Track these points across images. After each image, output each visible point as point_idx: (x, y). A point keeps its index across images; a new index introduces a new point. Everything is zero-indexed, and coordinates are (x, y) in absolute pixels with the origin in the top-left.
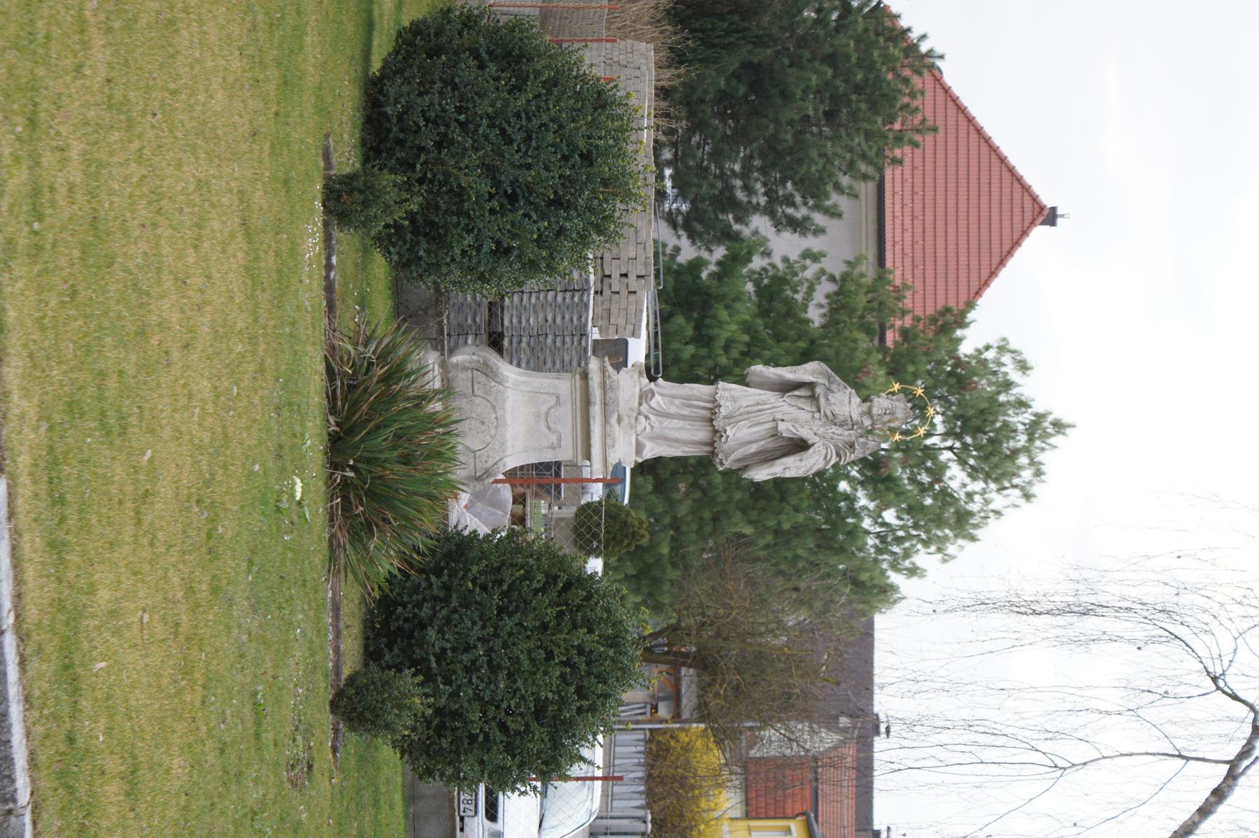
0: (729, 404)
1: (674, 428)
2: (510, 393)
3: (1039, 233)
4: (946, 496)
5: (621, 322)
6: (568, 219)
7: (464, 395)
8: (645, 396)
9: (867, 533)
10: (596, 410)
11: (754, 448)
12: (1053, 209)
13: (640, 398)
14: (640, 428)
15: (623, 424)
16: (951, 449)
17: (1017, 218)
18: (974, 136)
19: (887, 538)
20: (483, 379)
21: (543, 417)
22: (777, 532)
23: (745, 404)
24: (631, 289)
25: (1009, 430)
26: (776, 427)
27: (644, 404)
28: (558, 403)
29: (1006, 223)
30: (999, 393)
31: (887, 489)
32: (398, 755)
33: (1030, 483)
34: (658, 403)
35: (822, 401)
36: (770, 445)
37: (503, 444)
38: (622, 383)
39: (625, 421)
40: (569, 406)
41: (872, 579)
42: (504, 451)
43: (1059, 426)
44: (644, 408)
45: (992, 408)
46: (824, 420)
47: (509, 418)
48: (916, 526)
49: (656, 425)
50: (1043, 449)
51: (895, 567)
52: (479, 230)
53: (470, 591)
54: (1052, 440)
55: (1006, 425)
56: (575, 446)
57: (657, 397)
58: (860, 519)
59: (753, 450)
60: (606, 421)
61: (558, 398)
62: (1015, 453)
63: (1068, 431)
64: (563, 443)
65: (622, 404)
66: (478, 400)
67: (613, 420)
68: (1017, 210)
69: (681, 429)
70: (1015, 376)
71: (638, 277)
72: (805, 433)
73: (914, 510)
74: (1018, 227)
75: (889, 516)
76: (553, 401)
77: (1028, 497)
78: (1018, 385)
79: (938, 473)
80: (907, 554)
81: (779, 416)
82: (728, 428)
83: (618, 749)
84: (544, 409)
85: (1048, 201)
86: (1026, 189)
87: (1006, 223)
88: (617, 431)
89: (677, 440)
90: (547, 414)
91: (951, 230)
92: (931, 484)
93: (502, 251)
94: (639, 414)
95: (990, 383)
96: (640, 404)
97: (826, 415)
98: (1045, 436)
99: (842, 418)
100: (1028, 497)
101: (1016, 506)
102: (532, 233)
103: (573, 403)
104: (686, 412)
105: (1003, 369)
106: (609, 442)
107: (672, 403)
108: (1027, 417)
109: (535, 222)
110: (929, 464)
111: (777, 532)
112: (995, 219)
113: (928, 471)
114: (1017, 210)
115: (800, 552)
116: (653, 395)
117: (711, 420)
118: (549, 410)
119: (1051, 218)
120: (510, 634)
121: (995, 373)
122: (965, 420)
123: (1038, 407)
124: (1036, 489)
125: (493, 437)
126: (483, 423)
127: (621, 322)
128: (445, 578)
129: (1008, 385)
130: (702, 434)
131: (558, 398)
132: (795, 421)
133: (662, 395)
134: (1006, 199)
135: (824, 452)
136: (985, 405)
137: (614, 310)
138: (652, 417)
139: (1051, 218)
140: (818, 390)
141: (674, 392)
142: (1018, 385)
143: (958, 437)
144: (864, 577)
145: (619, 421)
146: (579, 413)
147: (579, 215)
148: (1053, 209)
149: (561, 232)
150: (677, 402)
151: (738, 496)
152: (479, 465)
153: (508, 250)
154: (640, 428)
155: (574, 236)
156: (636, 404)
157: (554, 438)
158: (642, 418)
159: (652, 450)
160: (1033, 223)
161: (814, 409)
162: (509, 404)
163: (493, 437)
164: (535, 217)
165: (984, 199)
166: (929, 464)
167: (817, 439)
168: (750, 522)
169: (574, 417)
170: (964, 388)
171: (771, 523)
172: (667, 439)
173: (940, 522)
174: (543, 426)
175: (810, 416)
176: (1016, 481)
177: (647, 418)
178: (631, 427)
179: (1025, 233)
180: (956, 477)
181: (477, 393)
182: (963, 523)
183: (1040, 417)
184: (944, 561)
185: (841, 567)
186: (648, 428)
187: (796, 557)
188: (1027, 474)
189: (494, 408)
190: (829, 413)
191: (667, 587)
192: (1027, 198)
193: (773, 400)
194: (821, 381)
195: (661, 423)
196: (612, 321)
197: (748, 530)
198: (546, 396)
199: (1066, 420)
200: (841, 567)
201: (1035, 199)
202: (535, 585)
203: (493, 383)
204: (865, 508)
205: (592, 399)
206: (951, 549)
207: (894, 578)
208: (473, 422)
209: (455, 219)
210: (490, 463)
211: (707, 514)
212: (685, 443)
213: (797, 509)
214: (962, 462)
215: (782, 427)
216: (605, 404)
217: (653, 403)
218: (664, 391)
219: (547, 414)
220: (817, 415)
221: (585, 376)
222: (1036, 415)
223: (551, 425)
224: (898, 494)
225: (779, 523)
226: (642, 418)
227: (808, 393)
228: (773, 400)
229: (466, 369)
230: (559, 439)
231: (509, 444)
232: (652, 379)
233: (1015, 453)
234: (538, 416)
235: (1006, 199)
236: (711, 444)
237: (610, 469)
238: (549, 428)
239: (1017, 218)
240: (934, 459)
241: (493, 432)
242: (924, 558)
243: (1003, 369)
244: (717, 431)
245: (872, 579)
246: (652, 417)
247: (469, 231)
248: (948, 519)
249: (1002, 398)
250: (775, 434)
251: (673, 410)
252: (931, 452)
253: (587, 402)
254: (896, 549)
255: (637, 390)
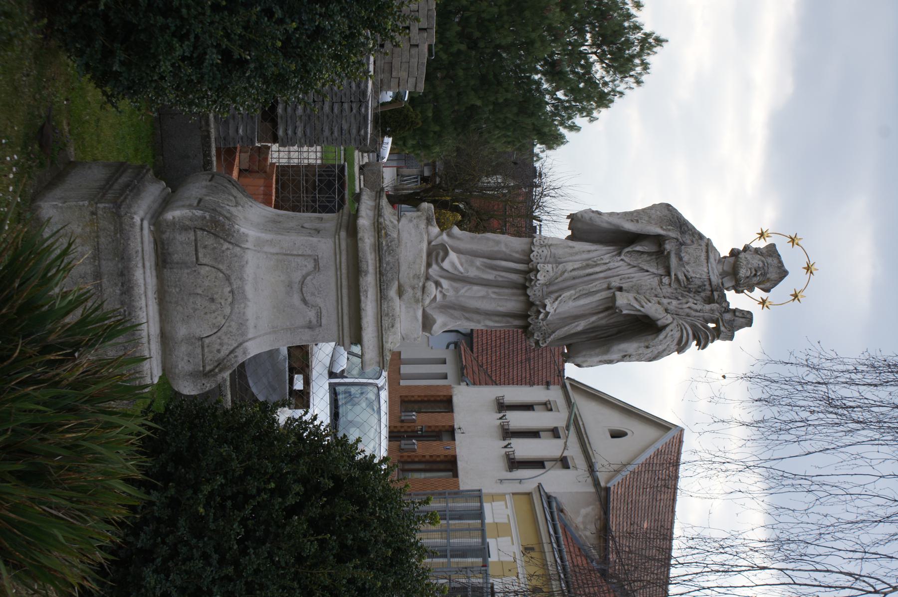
0: (549, 267)
1: (474, 296)
2: (250, 256)
4: (591, 82)
5: (403, 75)
6: (328, 16)
7: (183, 264)
8: (436, 253)
9: (548, 103)
10: (369, 281)
11: (581, 325)
13: (429, 255)
15: (405, 297)
16: (595, 53)
19: (559, 105)
20: (210, 241)
21: (296, 287)
22: (495, 104)
23: (570, 266)
24: (413, 42)
25: (629, 44)
26: (613, 298)
27: (434, 266)
28: (317, 267)
30: (625, 21)
31: (560, 79)
33: (640, 74)
35: (674, 261)
36: (603, 322)
37: (242, 325)
38: (405, 236)
39: (409, 293)
40: (331, 273)
41: (550, 131)
42: (243, 334)
43: (659, 41)
44: (434, 270)
45: (620, 31)
46: (674, 285)
47: (249, 289)
48: (575, 101)
49: (450, 294)
50: (649, 54)
51: (562, 124)
52: (197, 37)
53: (202, 518)
54: (655, 49)
55: (627, 40)
57: (453, 256)
58: (544, 96)
59: (580, 328)
60: (382, 296)
61: (316, 261)
62: (633, 57)
63: (663, 44)
64: (324, 321)
65: (404, 268)
66: (204, 270)
67: (392, 293)
69: (483, 297)
70: (633, 11)
71: (420, 29)
72: (652, 309)
73: (573, 91)
75: (560, 94)
76: (310, 266)
77: (639, 82)
78: (635, 17)
79: (588, 66)
80: (570, 118)
81: (615, 283)
82: (547, 302)
83: (405, 369)
84: (297, 276)
88: (398, 306)
89: (477, 311)
90: (302, 283)
92: (584, 74)
93: (232, 64)
94: (428, 278)
95: (620, 15)
96: (429, 265)
97: (677, 280)
98: (651, 47)
99: (698, 282)
100: (639, 82)
101: (631, 88)
102: (274, 38)
103: (338, 269)
104: (490, 276)
105: (627, 7)
106: (386, 323)
107: (472, 264)
108: (640, 35)
109: (281, 21)
110: (582, 62)
111: (495, 104)
113: (582, 66)
115: (509, 115)
116: (446, 254)
117: (525, 288)
118: (304, 277)
120: (257, 572)
121: (621, 9)
122: (604, 36)
123: (647, 29)
124: (644, 78)
125: (227, 318)
126: (212, 300)
127: (403, 75)
128: (172, 492)
129: (629, 16)
130: (511, 304)
131: (316, 261)
132: (637, 289)
133: (458, 251)
135: (677, 335)
136: (617, 28)
137: (396, 62)
138: (445, 283)
140: (668, 246)
141: (474, 246)
142: (635, 17)
143: (599, 46)
144: (546, 130)
145: (400, 293)
146: (345, 283)
147: (343, 9)
149: (318, 32)
150: (479, 262)
151: (472, 82)
152: (209, 357)
153: (242, 63)
155: (337, 38)
156: (423, 269)
157: (311, 314)
158: (431, 286)
161: (661, 271)
162: (250, 271)
163: (227, 318)
164: (279, 14)
166: (582, 62)
167: (669, 319)
168: (480, 98)
169: (339, 288)
170: (605, 19)
171: (492, 99)
172: (464, 309)
173: (589, 98)
174: (296, 300)
175: (656, 280)
176: (632, 73)
177: (438, 284)
178: (417, 301)
180: (598, 71)
181: (203, 260)
182: (604, 100)
183: (648, 35)
184: (591, 121)
186: (439, 297)
187: (506, 117)
188: (639, 69)
189: (228, 278)
190: (681, 277)
191: (431, 135)
193: (606, 258)
194: (672, 234)
195: (457, 290)
196: (394, 74)
197: (479, 103)
198: (299, 260)
199: (662, 37)
202: (291, 500)
203: (226, 245)
204: (546, 90)
205: (364, 266)
206: (595, 114)
207: (562, 130)
208: (199, 300)
209: (160, 20)
210: (225, 351)
211: (454, 93)
212: (488, 314)
213: (507, 91)
214: (602, 62)
215: (622, 300)
216: (380, 274)
217: (446, 265)
218: (462, 245)
219: (302, 283)
220: (666, 280)
222: (645, 34)
223: (308, 298)
224: (566, 82)
225: (497, 99)
226: (431, 286)
228: (606, 258)
229: (185, 228)
230: (319, 316)
231: (251, 323)
233: (633, 57)
234: (290, 285)
237: (388, 357)
238: (304, 301)
240: (587, 60)
241: (227, 310)
242: (579, 120)
243: (627, 7)
244: (531, 304)
245: (550, 131)
246: (445, 283)
247: (182, 38)
248: (597, 97)
249: (626, 24)
250: (610, 306)
251: (473, 273)
252: (584, 56)
253: (355, 270)
254: (563, 113)
255: (425, 246)
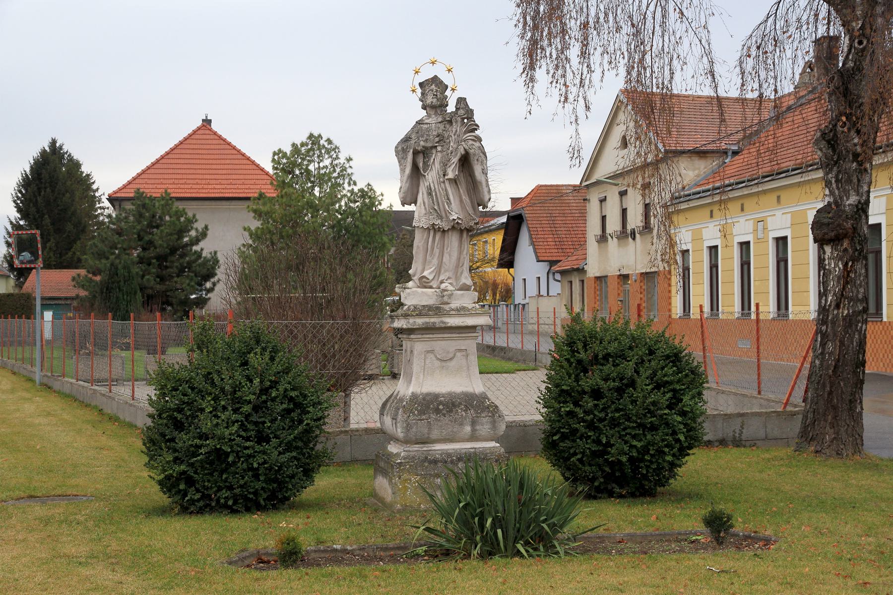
3: (214, 126)
11: (465, 198)
12: (203, 120)
13: (426, 287)
14: (450, 288)
17: (208, 137)
18: (170, 156)
21: (444, 364)
26: (449, 180)
28: (432, 352)
29: (210, 142)
32: (687, 458)
34: (430, 273)
49: (447, 274)
56: (466, 338)
57: (426, 273)
61: (428, 352)
68: (204, 137)
69: (450, 255)
74: (212, 137)
85: (200, 123)
86: (194, 132)
87: (210, 142)
89: (459, 259)
91: (214, 167)
96: (431, 287)
103: (432, 340)
104: (437, 251)
107: (430, 262)
112: (208, 147)
114: (204, 137)
116: (424, 277)
117: (444, 231)
118: (438, 359)
119: (207, 122)
131: (428, 352)
133: (423, 271)
134: (199, 142)
139: (207, 122)
148: (203, 120)
154: (450, 288)
156: (433, 290)
157: (459, 354)
159: (466, 278)
160: (211, 130)
161: (434, 151)
165: (200, 152)
169: (443, 339)
172: (457, 267)
177: (442, 282)
179: (215, 133)
185: (193, 296)
192: (199, 132)
195: (445, 271)
198: (428, 362)
200: (193, 296)
201: (199, 129)
217: (431, 277)
218: (420, 268)
220: (439, 148)
221: (410, 331)
227: (421, 156)
230: (460, 350)
232: (409, 278)
235: (199, 142)
236: (461, 231)
238: (451, 359)
239: (208, 137)
244: (453, 228)
251: (435, 261)
255: (420, 290)
